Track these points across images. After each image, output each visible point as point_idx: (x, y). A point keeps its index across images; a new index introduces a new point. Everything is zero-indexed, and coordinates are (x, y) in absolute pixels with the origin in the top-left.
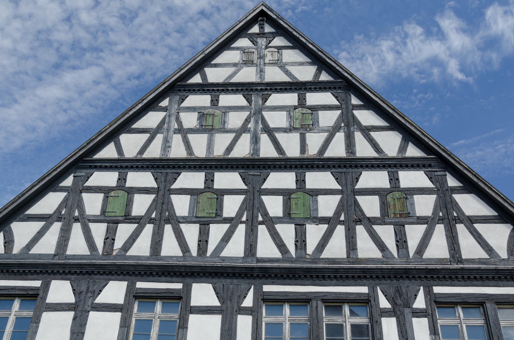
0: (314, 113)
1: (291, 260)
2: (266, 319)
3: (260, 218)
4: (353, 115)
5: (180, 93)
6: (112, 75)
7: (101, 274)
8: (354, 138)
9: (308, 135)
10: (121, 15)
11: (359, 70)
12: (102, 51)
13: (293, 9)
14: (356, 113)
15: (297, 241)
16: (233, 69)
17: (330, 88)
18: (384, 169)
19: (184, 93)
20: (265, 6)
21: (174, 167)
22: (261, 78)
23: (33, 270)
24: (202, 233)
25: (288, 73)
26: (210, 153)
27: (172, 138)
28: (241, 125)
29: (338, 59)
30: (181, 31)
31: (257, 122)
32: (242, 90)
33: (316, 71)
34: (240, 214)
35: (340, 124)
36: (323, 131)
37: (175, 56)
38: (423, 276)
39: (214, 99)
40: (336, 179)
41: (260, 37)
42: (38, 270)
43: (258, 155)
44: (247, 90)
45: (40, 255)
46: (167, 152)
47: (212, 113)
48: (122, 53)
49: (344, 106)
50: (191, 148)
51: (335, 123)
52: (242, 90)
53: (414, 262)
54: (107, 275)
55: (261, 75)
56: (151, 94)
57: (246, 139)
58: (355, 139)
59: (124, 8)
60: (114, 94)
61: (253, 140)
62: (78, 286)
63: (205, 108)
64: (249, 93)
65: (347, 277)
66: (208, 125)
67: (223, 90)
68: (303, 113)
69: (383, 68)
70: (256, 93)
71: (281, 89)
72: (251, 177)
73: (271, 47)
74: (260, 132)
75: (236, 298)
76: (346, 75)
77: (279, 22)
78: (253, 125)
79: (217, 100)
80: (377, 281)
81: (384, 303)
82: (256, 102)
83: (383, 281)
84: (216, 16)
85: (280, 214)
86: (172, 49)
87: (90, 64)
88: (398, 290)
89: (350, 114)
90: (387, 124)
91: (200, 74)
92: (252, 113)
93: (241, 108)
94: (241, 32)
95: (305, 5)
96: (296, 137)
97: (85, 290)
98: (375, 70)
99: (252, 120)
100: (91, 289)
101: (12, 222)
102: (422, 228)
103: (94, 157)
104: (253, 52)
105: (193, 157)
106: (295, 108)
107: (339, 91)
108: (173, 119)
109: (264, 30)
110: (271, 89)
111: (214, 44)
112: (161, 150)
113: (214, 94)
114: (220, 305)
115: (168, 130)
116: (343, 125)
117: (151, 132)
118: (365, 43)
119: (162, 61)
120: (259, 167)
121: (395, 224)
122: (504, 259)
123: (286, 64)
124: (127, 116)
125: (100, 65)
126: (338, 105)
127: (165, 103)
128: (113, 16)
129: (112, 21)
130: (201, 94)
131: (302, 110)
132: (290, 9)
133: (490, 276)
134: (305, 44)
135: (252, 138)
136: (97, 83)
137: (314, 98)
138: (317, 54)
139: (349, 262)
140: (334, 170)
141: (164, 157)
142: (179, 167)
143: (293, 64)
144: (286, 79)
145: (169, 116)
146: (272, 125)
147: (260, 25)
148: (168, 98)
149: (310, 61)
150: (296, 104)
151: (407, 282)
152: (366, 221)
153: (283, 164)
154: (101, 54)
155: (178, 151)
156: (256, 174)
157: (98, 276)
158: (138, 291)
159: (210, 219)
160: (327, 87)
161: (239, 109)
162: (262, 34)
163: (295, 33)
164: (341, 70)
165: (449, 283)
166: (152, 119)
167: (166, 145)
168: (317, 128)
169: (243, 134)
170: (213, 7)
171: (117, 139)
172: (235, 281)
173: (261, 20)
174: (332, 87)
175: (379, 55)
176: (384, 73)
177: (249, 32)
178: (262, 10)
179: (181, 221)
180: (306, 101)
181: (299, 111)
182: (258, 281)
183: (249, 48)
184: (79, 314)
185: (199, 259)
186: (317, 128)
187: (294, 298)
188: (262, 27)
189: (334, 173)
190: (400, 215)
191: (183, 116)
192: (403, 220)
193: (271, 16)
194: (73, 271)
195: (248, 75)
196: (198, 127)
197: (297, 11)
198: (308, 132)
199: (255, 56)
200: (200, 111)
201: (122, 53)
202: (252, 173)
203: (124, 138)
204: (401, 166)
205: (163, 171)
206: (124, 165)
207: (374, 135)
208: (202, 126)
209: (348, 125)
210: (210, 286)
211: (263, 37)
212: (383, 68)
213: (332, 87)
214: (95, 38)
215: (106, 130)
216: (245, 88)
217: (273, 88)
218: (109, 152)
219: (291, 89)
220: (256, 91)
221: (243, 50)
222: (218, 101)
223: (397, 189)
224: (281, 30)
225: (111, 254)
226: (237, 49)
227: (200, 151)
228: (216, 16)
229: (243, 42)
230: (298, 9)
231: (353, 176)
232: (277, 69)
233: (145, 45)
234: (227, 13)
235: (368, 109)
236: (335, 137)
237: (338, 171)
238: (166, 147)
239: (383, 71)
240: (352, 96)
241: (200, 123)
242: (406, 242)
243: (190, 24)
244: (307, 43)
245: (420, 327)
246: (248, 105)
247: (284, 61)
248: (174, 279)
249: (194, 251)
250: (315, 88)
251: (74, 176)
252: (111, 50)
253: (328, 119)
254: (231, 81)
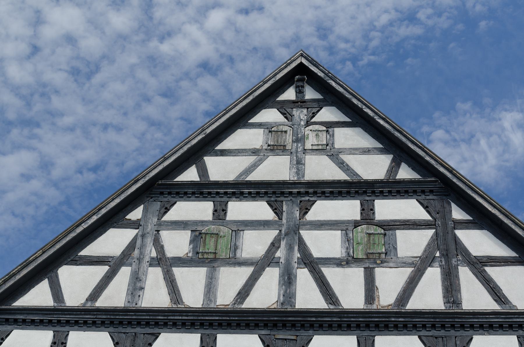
4: (456, 239)
5: (161, 198)
6: (53, 164)
8: (457, 277)
9: (379, 272)
10: (73, 68)
11: (465, 160)
12: (38, 125)
13: (354, 59)
14: (459, 233)
16: (252, 159)
17: (415, 192)
18: (511, 331)
19: (169, 198)
20: (305, 58)
21: (148, 324)
22: (297, 173)
25: (343, 166)
26: (211, 301)
27: (146, 274)
28: (263, 253)
29: (429, 142)
30: (169, 94)
31: (290, 248)
32: (266, 193)
33: (392, 163)
35: (433, 253)
36: (404, 264)
37: (158, 135)
39: (219, 208)
41: (298, 107)
43: (293, 305)
44: (274, 193)
46: (137, 297)
47: (215, 232)
48: (71, 129)
49: (439, 222)
50: (179, 291)
51: (425, 251)
52: (266, 193)
55: (298, 169)
56: (113, 199)
57: (271, 277)
58: (459, 280)
59: (78, 58)
60: (53, 195)
61: (284, 279)
63: (203, 223)
64: (279, 199)
66: (207, 254)
67: (234, 194)
68: (370, 234)
69: (506, 156)
70: (289, 199)
71: (332, 193)
72: (280, 343)
73: (316, 123)
74: (296, 265)
76: (442, 169)
77: (329, 84)
78: (285, 252)
79: (223, 210)
82: (290, 213)
84: (228, 70)
86: (152, 123)
87: (17, 147)
89: (450, 236)
90: (513, 254)
91: (197, 167)
92: (283, 232)
93: (263, 225)
94: (267, 98)
95: (373, 54)
96: (356, 275)
98: (492, 160)
99: (283, 244)
101: (60, 265)
103: (175, 180)
104: (286, 132)
106: (356, 224)
107: (431, 197)
108: (149, 241)
109: (304, 96)
110: (315, 193)
111: (220, 118)
112: (127, 294)
113: (219, 199)
115: (140, 260)
116: (438, 254)
117: (111, 264)
118: (474, 116)
119: (136, 143)
120: (294, 326)
123: (341, 151)
124: (73, 235)
125: (34, 149)
126: (429, 220)
127: (136, 214)
128: (60, 70)
129: (58, 78)
130: (198, 199)
131: (368, 229)
132: (349, 60)
134: (373, 118)
135: (282, 276)
136: (26, 177)
137: (387, 209)
138: (393, 135)
140: (423, 333)
141: (132, 306)
142: (157, 324)
143: (353, 151)
144: (341, 176)
145: (143, 236)
146: (317, 252)
147: (297, 87)
148: (142, 206)
149: (381, 146)
150: (358, 217)
154: (37, 131)
155: (155, 296)
156: (289, 337)
160: (410, 190)
161: (261, 225)
162: (300, 103)
163: (355, 101)
164: (433, 162)
166: (113, 242)
167: (136, 285)
168: (394, 258)
169: (267, 269)
170: (222, 56)
171: (53, 274)
173: (298, 80)
174: (419, 190)
175: (499, 136)
176: (508, 164)
177: (278, 99)
178: (301, 63)
180: (374, 213)
181: (362, 229)
183: (278, 125)
186: (394, 258)
188: (300, 92)
189: (423, 338)
191: (166, 235)
193: (316, 74)
195: (276, 169)
196: (190, 255)
197: (361, 63)
198: (379, 266)
199: (289, 138)
200: (194, 228)
201: (71, 129)
202: (281, 337)
203: (66, 273)
205: (129, 330)
206: (63, 318)
207: (492, 271)
208: (198, 253)
209: (446, 255)
211: (301, 107)
212: (506, 156)
213: (419, 190)
214: (29, 105)
215: (37, 258)
216: (270, 191)
217: (319, 191)
218: (39, 296)
219: (348, 193)
220: (292, 195)
221: (269, 128)
222: (225, 211)
224: (332, 96)
226: (259, 125)
227: (193, 298)
228: (228, 70)
229: (270, 115)
230: (362, 60)
231: (458, 343)
232: (325, 160)
233: (108, 116)
234: (246, 67)
235: (481, 228)
236: (425, 276)
237: (430, 333)
238: (135, 289)
239: (507, 161)
240: (453, 205)
241: (193, 248)
243: (185, 84)
244: (376, 118)
246: (277, 219)
247: (336, 146)
252: (53, 124)
253: (413, 243)
254: (248, 179)
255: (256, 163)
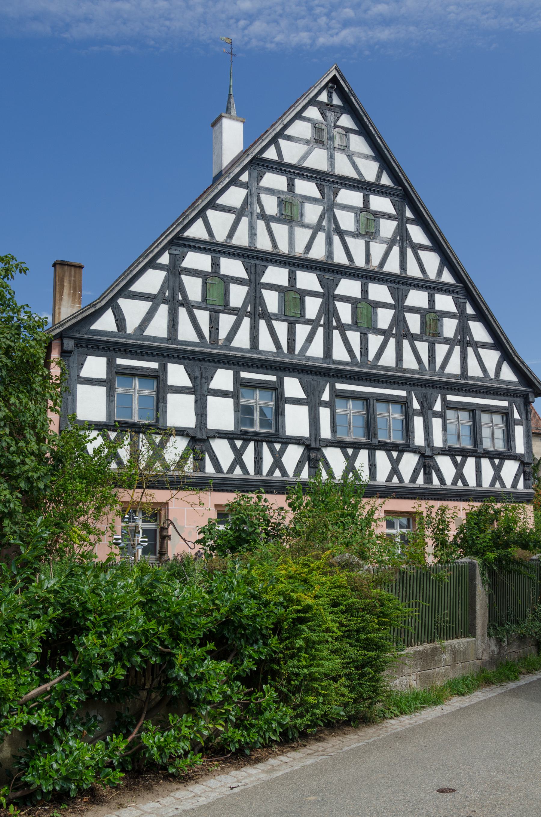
0: (377, 219)
1: (285, 356)
2: (119, 390)
3: (335, 324)
7: (210, 362)
9: (372, 244)
15: (361, 348)
24: (213, 320)
31: (329, 221)
32: (316, 178)
34: (318, 317)
38: (442, 386)
40: (391, 294)
42: (155, 353)
45: (154, 337)
54: (215, 363)
62: (192, 371)
65: (394, 382)
75: (317, 393)
80: (413, 388)
81: (416, 405)
83: (416, 388)
85: (350, 322)
88: (425, 396)
97: (199, 376)
99: (326, 216)
100: (204, 375)
102: (446, 347)
105: (277, 251)
123: (353, 153)
130: (278, 173)
133: (482, 391)
140: (390, 285)
142: (267, 260)
144: (353, 174)
152: (410, 336)
153: (351, 272)
157: (208, 363)
158: (243, 381)
159: (295, 319)
165: (456, 393)
172: (315, 378)
179: (273, 317)
182: (332, 379)
184: (199, 398)
185: (290, 356)
187: (358, 396)
188: (330, 97)
190: (433, 334)
192: (434, 339)
194: (186, 356)
200: (279, 196)
207: (421, 253)
210: (297, 380)
216: (318, 177)
223: (432, 310)
225: (217, 344)
242: (435, 358)
249: (492, 376)
250: (382, 192)
251: (170, 254)
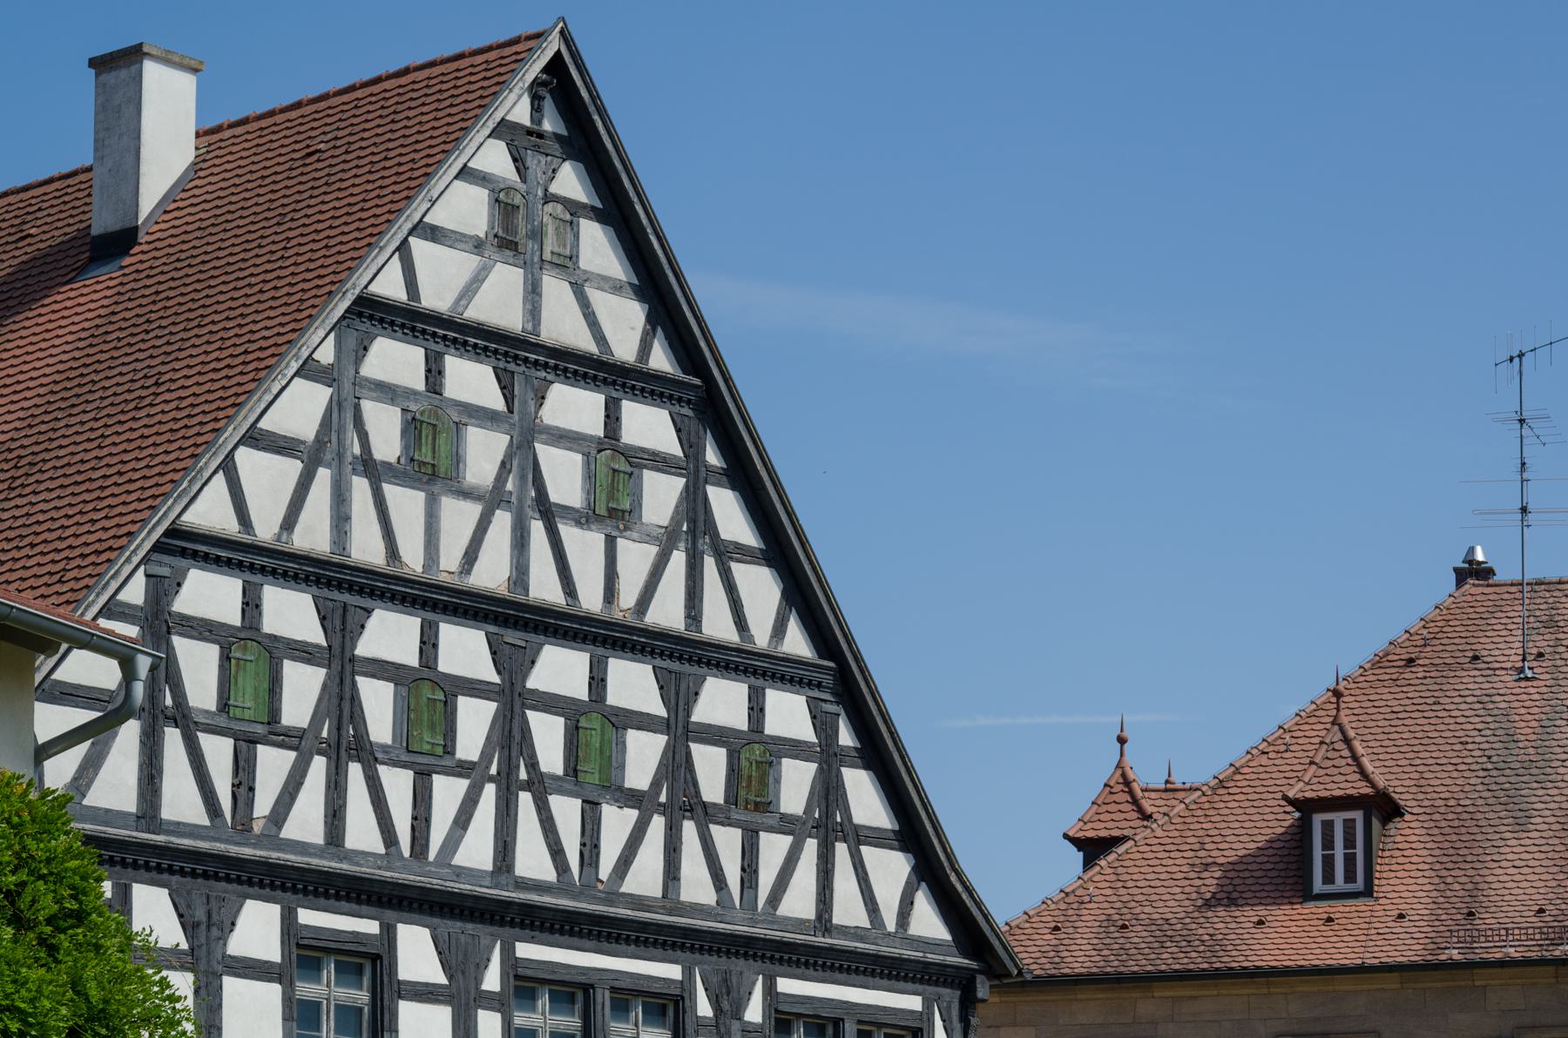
3: (523, 775)
23: (153, 862)
45: (107, 811)
53: (763, 921)
62: (189, 906)
68: (615, 471)
75: (473, 968)
97: (204, 919)
100: (215, 917)
102: (462, 785)
114: (445, 982)
121: (237, 737)
122: (889, 934)
123: (589, 277)
134: (644, 230)
139: (663, 907)
140: (658, 662)
142: (372, 594)
151: (741, 961)
158: (304, 934)
187: (567, 978)
204: (773, 676)
206: (259, 561)
210: (426, 932)
217: (562, 364)
245: (489, 1025)
248: (365, 909)
250: (643, 390)
251: (147, 576)
255: (478, 273)
